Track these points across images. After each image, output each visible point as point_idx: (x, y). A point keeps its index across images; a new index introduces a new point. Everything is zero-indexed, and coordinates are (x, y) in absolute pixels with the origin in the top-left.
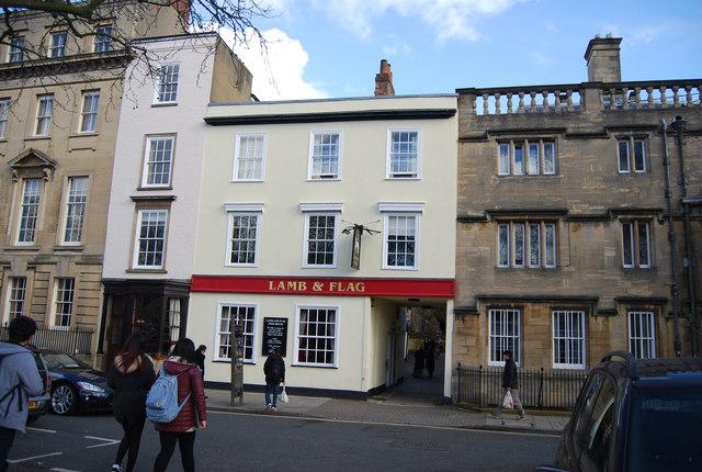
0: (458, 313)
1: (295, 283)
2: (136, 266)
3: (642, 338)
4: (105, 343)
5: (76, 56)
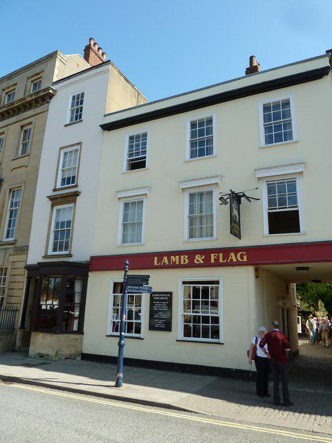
1: (177, 257)
2: (50, 252)
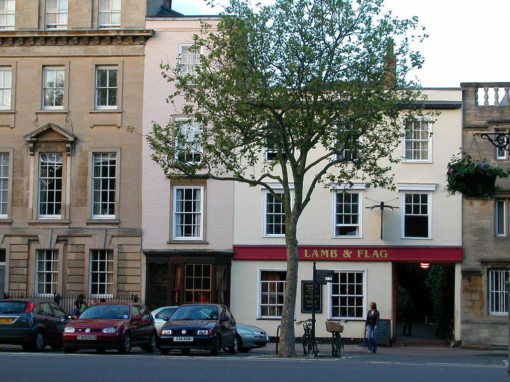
0: (466, 274)
1: (327, 251)
3: (504, 292)
4: (112, 351)
5: (90, 32)
